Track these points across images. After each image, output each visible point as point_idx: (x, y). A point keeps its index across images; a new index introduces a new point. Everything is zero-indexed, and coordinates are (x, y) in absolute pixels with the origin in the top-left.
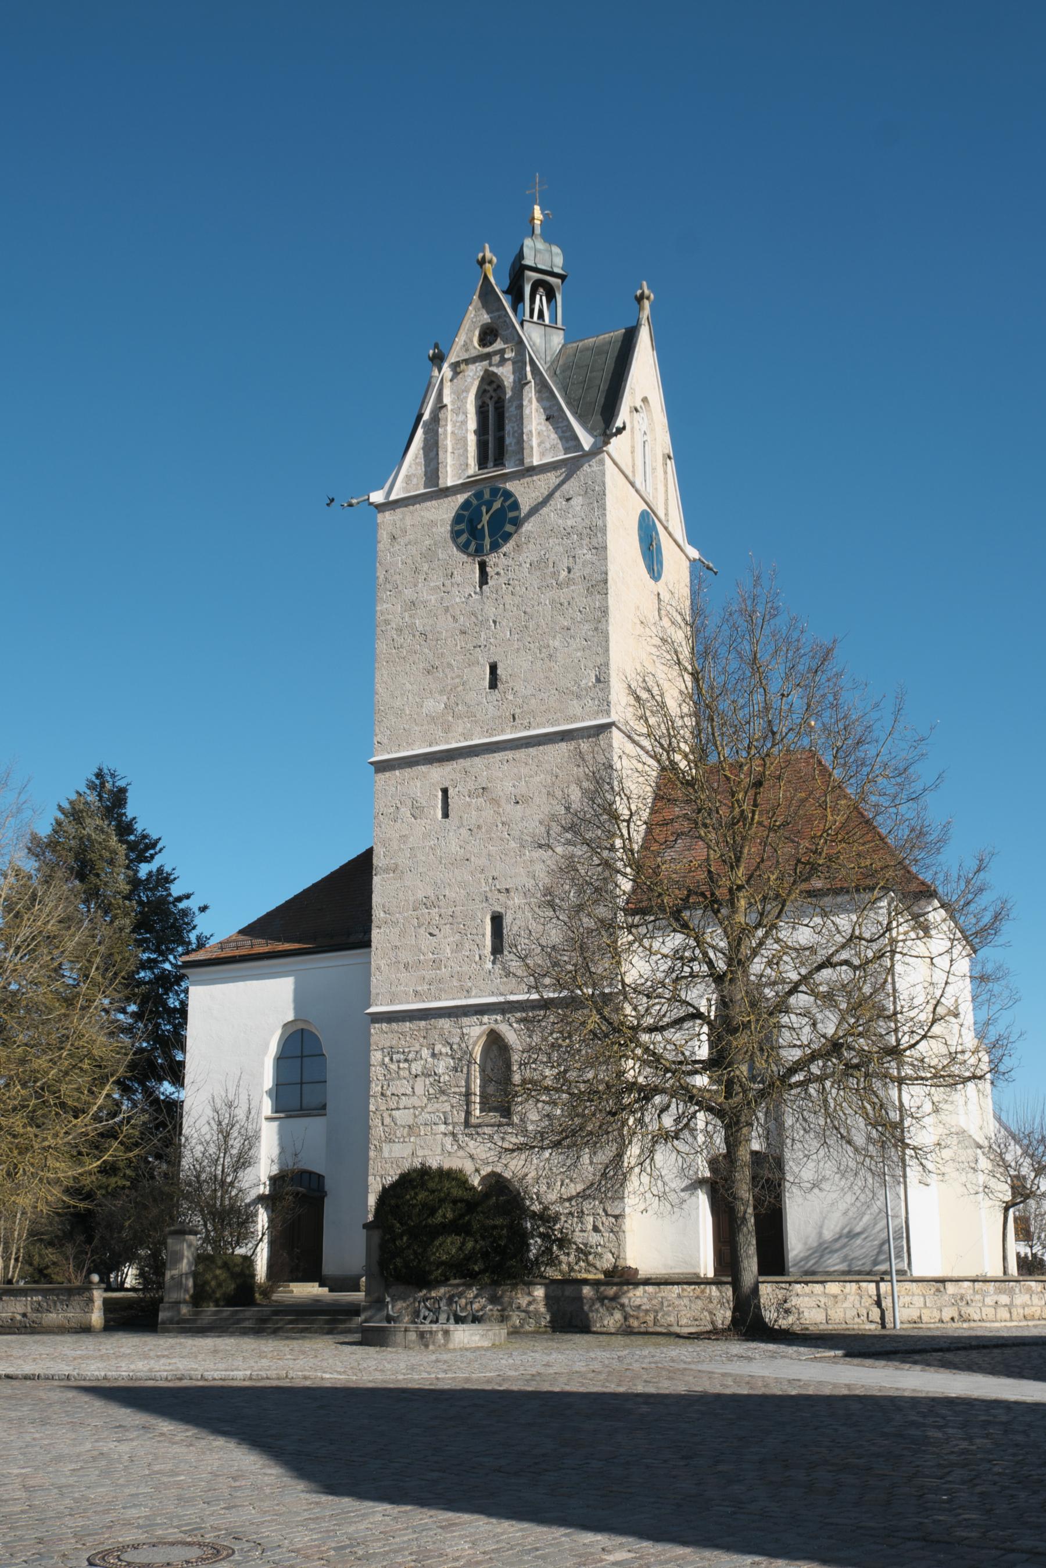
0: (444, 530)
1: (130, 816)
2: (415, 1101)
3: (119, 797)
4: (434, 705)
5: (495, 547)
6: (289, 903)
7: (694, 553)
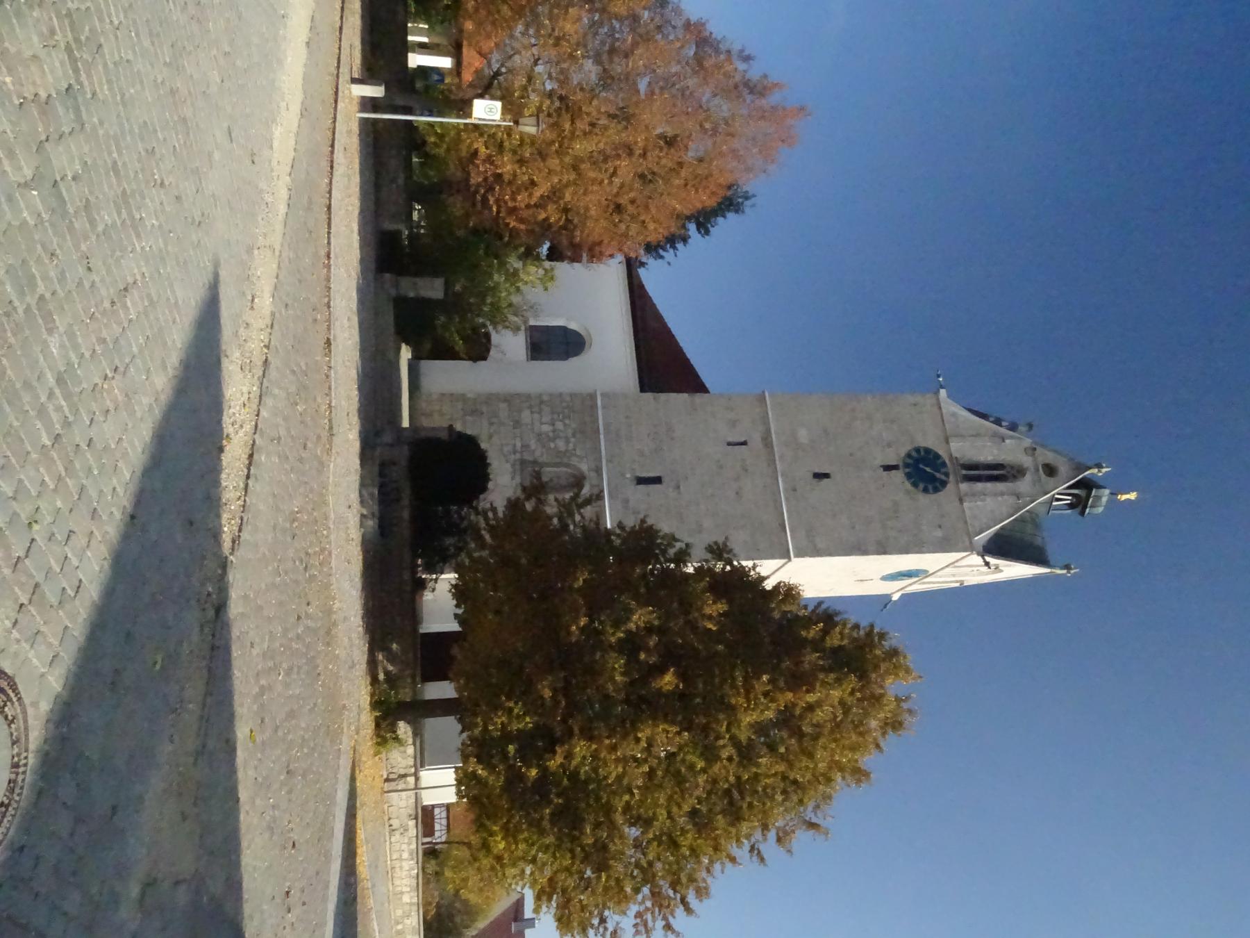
0: (924, 442)
1: (867, 760)
2: (537, 424)
3: (738, 209)
4: (803, 435)
5: (909, 476)
6: (669, 331)
7: (895, 597)
